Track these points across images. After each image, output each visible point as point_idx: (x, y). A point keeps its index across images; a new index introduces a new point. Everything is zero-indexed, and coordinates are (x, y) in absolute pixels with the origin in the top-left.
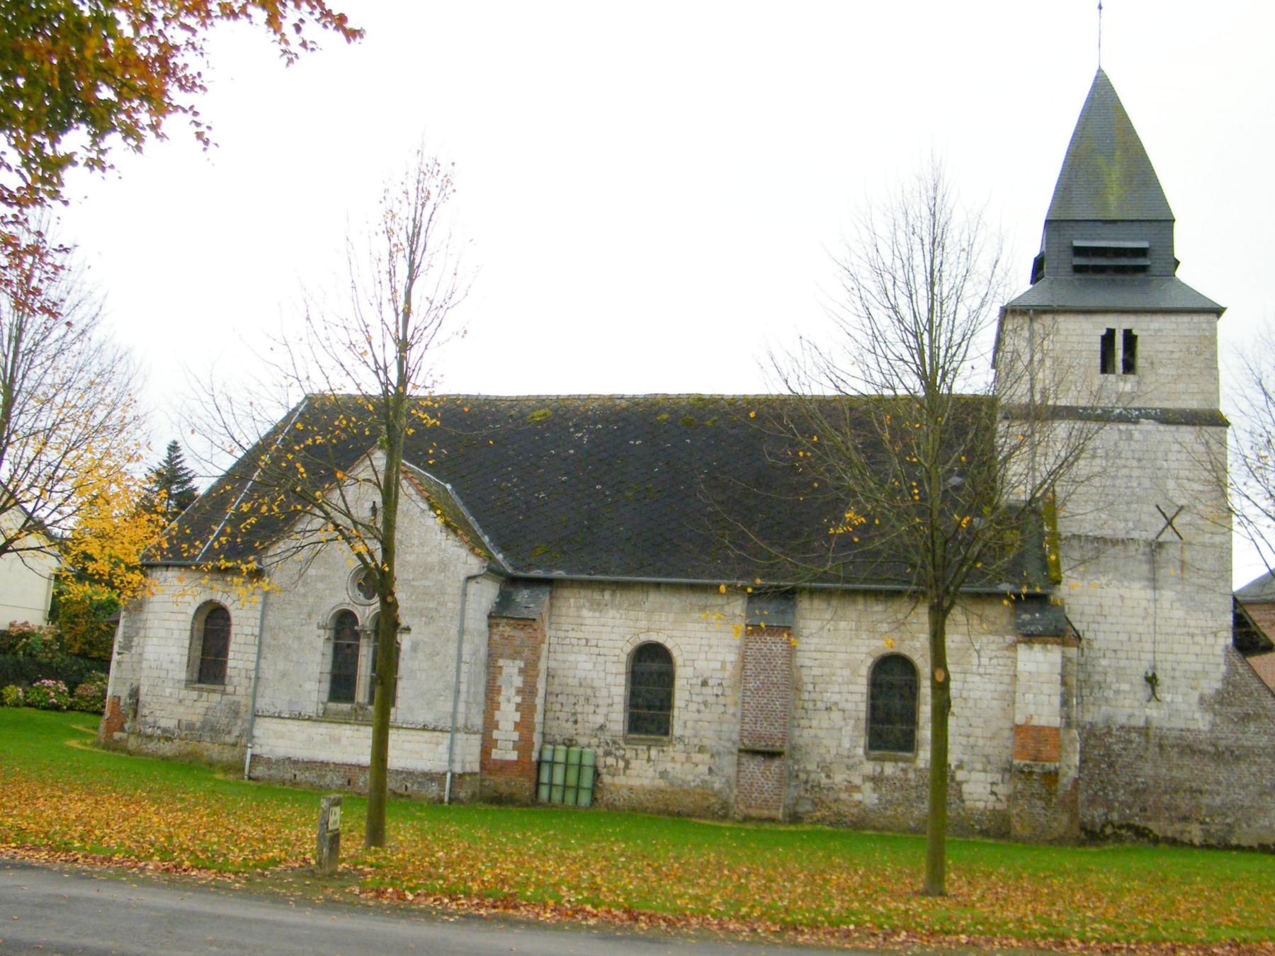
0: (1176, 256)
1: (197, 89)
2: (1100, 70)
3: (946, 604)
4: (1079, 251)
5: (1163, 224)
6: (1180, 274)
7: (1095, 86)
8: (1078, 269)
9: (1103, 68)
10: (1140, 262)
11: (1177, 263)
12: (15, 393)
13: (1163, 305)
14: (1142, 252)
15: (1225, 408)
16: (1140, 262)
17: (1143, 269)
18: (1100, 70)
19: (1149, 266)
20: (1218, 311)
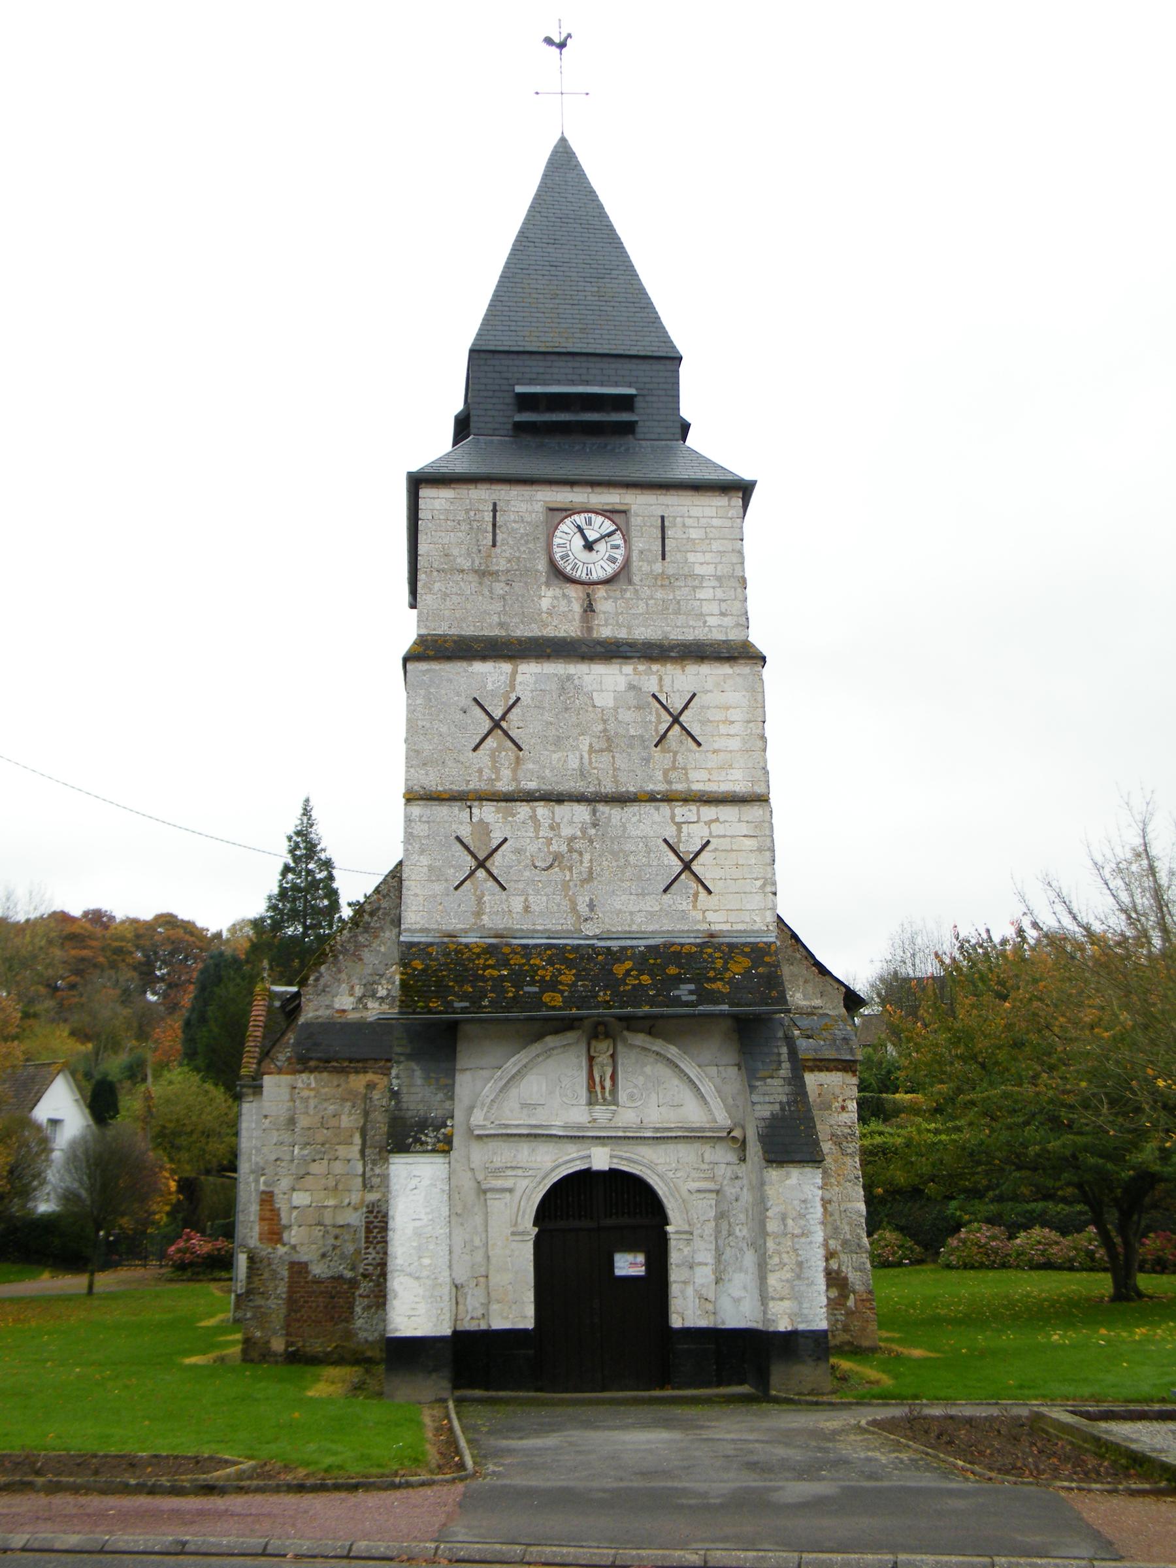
0: (685, 412)
1: (482, 1198)
2: (563, 140)
3: (312, 1064)
4: (526, 402)
5: (658, 366)
6: (693, 440)
7: (555, 153)
8: (520, 429)
9: (565, 135)
10: (625, 417)
11: (685, 428)
12: (126, 1263)
13: (654, 475)
14: (625, 403)
15: (758, 638)
16: (625, 417)
17: (628, 429)
18: (563, 140)
19: (636, 422)
20: (743, 489)
